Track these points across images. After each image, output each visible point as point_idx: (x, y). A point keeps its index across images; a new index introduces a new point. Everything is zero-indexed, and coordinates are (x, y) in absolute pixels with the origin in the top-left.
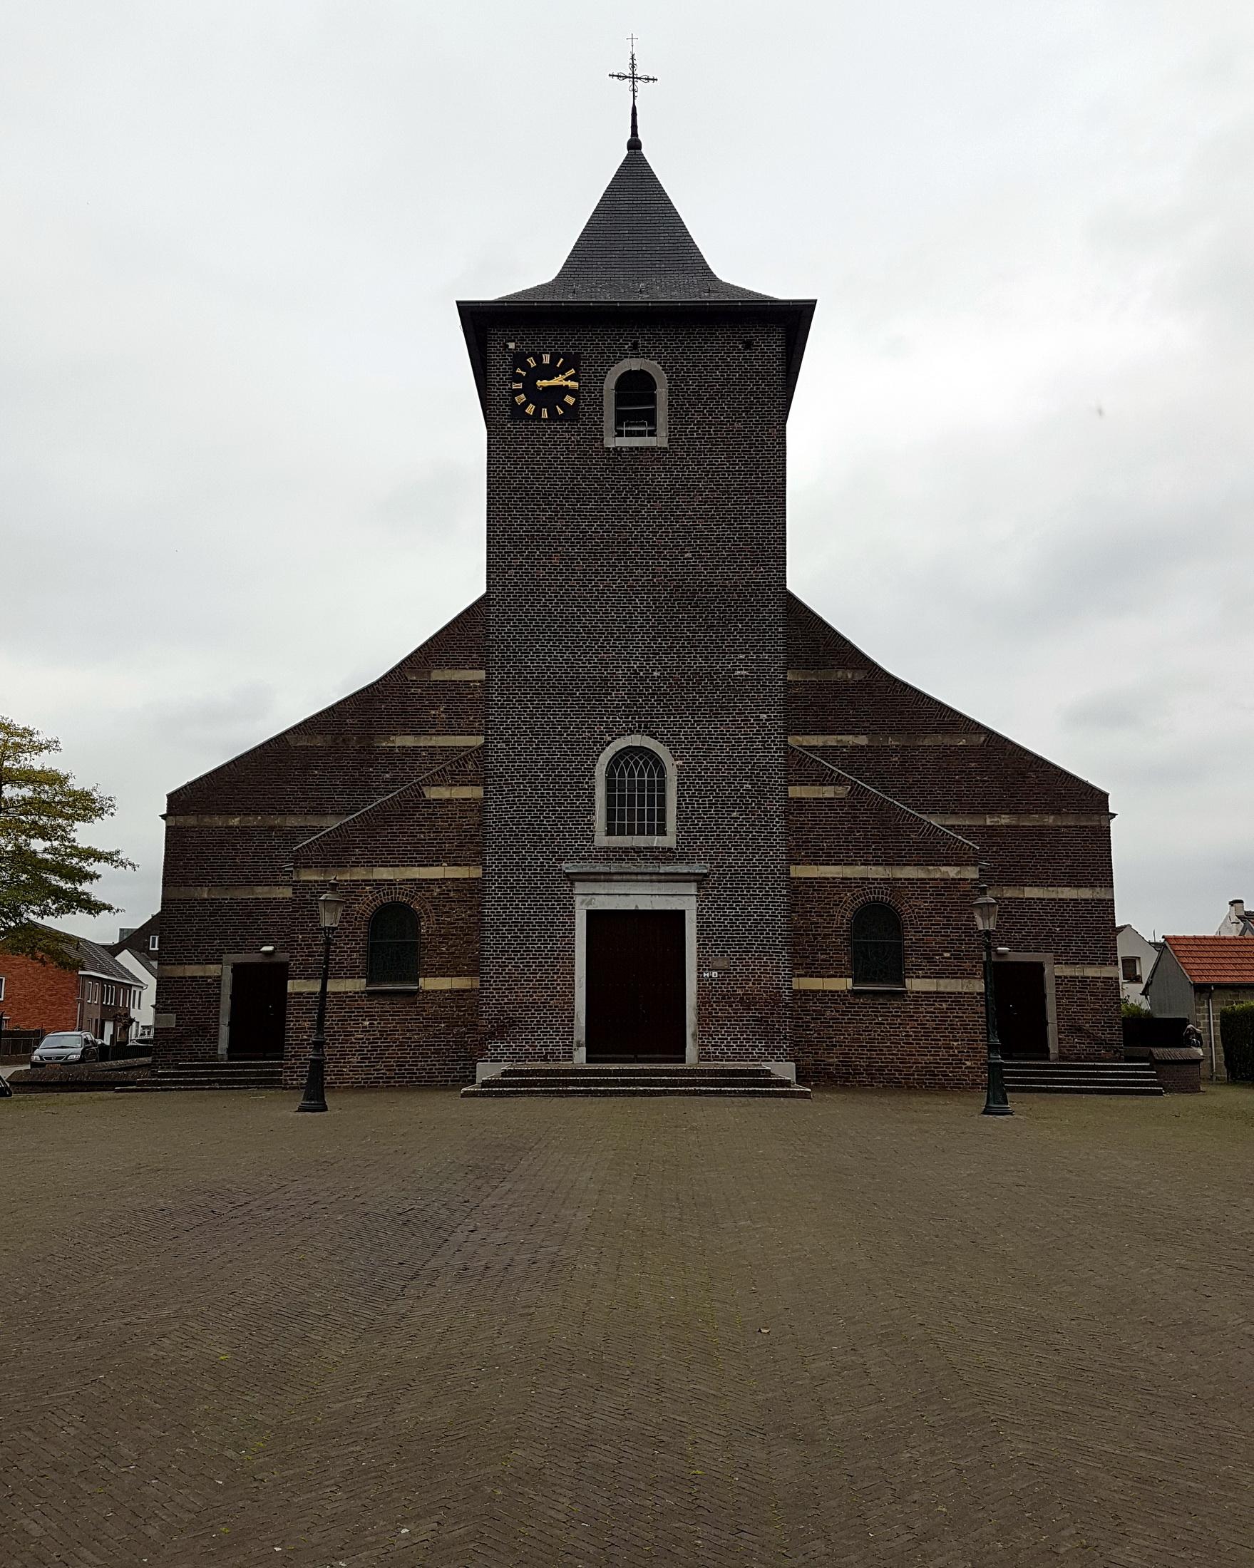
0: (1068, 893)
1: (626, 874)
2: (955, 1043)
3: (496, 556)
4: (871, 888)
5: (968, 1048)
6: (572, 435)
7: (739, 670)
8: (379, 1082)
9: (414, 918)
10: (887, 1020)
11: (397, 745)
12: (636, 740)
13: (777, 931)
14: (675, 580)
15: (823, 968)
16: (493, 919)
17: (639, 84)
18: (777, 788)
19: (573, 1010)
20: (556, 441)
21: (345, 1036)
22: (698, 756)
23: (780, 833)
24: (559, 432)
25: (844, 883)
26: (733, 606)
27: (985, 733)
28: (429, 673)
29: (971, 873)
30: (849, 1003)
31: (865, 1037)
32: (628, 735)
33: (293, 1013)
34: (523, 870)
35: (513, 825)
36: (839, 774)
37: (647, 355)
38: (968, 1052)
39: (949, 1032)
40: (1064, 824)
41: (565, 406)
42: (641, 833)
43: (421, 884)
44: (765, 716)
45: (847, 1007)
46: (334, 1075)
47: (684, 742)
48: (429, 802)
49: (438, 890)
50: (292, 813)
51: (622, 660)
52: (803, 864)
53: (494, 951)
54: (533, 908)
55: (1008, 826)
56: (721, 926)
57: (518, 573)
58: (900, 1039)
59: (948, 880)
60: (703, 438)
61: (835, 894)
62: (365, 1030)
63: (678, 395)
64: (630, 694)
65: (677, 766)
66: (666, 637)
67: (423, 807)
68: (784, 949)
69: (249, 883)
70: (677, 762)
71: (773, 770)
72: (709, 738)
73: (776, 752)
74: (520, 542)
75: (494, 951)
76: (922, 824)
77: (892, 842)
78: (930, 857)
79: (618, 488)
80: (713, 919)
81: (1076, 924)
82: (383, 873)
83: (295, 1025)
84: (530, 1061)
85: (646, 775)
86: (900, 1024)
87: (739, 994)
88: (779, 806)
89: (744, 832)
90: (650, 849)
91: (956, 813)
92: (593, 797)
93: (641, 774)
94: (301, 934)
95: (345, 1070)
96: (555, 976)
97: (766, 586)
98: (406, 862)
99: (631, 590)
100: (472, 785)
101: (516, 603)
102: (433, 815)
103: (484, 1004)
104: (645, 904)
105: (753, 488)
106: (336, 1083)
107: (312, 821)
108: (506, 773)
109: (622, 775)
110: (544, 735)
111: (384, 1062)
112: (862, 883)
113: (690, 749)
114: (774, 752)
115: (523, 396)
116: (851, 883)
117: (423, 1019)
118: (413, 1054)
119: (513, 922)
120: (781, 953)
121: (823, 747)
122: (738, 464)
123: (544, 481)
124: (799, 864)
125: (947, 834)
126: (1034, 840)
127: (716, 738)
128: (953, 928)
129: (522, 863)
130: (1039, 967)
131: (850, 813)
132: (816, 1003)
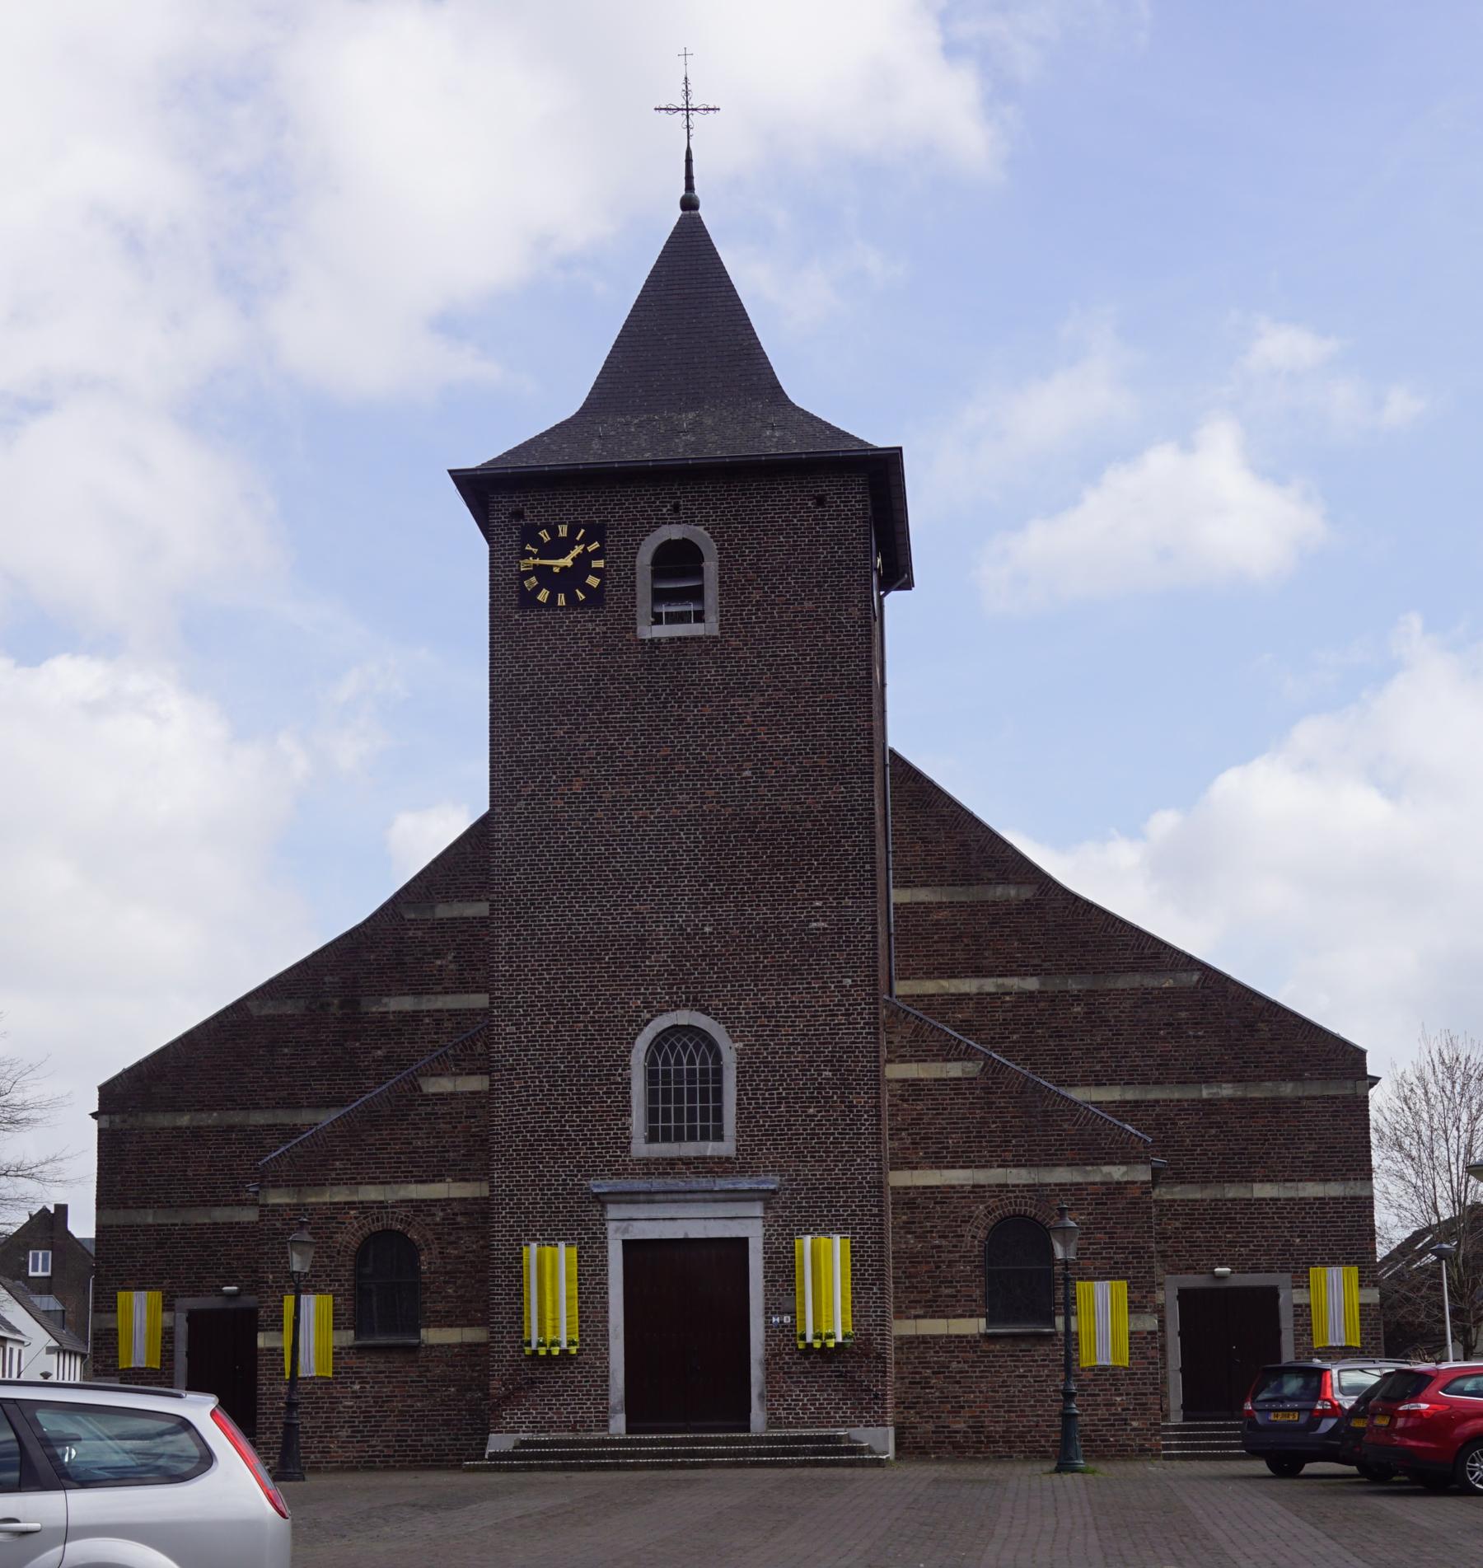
0: (1311, 1190)
1: (672, 1192)
2: (1118, 1399)
3: (502, 784)
4: (1010, 1197)
5: (1135, 1404)
6: (596, 625)
8: (375, 1462)
9: (412, 1251)
10: (1031, 1371)
12: (684, 1017)
13: (867, 1261)
14: (731, 806)
15: (947, 1306)
16: (504, 1254)
18: (866, 1076)
19: (607, 1367)
20: (576, 634)
21: (330, 1403)
23: (869, 1134)
24: (580, 622)
26: (806, 838)
28: (432, 908)
29: (1142, 1174)
30: (981, 1352)
31: (1001, 1395)
32: (673, 1010)
33: (265, 1375)
34: (540, 1190)
35: (527, 1132)
36: (968, 1045)
37: (690, 519)
38: (1134, 1409)
39: (1111, 1385)
40: (1306, 1094)
41: (587, 589)
42: (692, 1138)
43: (419, 1206)
44: (849, 981)
45: (979, 1357)
46: (319, 1452)
47: (745, 1018)
48: (427, 1098)
49: (441, 1214)
50: (257, 1107)
52: (922, 1168)
53: (506, 1294)
57: (530, 804)
58: (1047, 1396)
59: (1111, 1183)
60: (765, 622)
61: (963, 1207)
62: (356, 1396)
63: (731, 569)
64: (675, 957)
65: (737, 1050)
66: (720, 880)
67: (419, 1105)
68: (875, 1284)
69: (205, 1203)
70: (737, 1045)
74: (531, 765)
76: (1078, 1110)
77: (1038, 1135)
78: (1090, 1152)
79: (655, 691)
80: (784, 1248)
81: (1322, 1232)
82: (371, 1193)
83: (268, 1389)
84: (555, 1431)
85: (698, 1062)
86: (1047, 1376)
88: (869, 1098)
89: (823, 1134)
90: (703, 1159)
92: (628, 1093)
93: (691, 1061)
95: (332, 1446)
97: (848, 811)
98: (399, 1177)
99: (674, 821)
100: (481, 1074)
101: (527, 843)
103: (497, 1361)
104: (696, 1231)
105: (830, 684)
106: (322, 1462)
107: (284, 1117)
108: (517, 1065)
109: (666, 1062)
111: (381, 1436)
112: (1000, 1191)
113: (753, 1027)
114: (862, 1028)
115: (533, 579)
116: (985, 1192)
117: (428, 1381)
118: (417, 1426)
120: (872, 1289)
121: (978, 994)
122: (809, 654)
123: (561, 686)
125: (1111, 1122)
126: (1267, 1117)
127: (786, 1012)
128: (1117, 1248)
129: (540, 1181)
130: (1272, 1293)
131: (983, 1098)
132: (937, 1352)
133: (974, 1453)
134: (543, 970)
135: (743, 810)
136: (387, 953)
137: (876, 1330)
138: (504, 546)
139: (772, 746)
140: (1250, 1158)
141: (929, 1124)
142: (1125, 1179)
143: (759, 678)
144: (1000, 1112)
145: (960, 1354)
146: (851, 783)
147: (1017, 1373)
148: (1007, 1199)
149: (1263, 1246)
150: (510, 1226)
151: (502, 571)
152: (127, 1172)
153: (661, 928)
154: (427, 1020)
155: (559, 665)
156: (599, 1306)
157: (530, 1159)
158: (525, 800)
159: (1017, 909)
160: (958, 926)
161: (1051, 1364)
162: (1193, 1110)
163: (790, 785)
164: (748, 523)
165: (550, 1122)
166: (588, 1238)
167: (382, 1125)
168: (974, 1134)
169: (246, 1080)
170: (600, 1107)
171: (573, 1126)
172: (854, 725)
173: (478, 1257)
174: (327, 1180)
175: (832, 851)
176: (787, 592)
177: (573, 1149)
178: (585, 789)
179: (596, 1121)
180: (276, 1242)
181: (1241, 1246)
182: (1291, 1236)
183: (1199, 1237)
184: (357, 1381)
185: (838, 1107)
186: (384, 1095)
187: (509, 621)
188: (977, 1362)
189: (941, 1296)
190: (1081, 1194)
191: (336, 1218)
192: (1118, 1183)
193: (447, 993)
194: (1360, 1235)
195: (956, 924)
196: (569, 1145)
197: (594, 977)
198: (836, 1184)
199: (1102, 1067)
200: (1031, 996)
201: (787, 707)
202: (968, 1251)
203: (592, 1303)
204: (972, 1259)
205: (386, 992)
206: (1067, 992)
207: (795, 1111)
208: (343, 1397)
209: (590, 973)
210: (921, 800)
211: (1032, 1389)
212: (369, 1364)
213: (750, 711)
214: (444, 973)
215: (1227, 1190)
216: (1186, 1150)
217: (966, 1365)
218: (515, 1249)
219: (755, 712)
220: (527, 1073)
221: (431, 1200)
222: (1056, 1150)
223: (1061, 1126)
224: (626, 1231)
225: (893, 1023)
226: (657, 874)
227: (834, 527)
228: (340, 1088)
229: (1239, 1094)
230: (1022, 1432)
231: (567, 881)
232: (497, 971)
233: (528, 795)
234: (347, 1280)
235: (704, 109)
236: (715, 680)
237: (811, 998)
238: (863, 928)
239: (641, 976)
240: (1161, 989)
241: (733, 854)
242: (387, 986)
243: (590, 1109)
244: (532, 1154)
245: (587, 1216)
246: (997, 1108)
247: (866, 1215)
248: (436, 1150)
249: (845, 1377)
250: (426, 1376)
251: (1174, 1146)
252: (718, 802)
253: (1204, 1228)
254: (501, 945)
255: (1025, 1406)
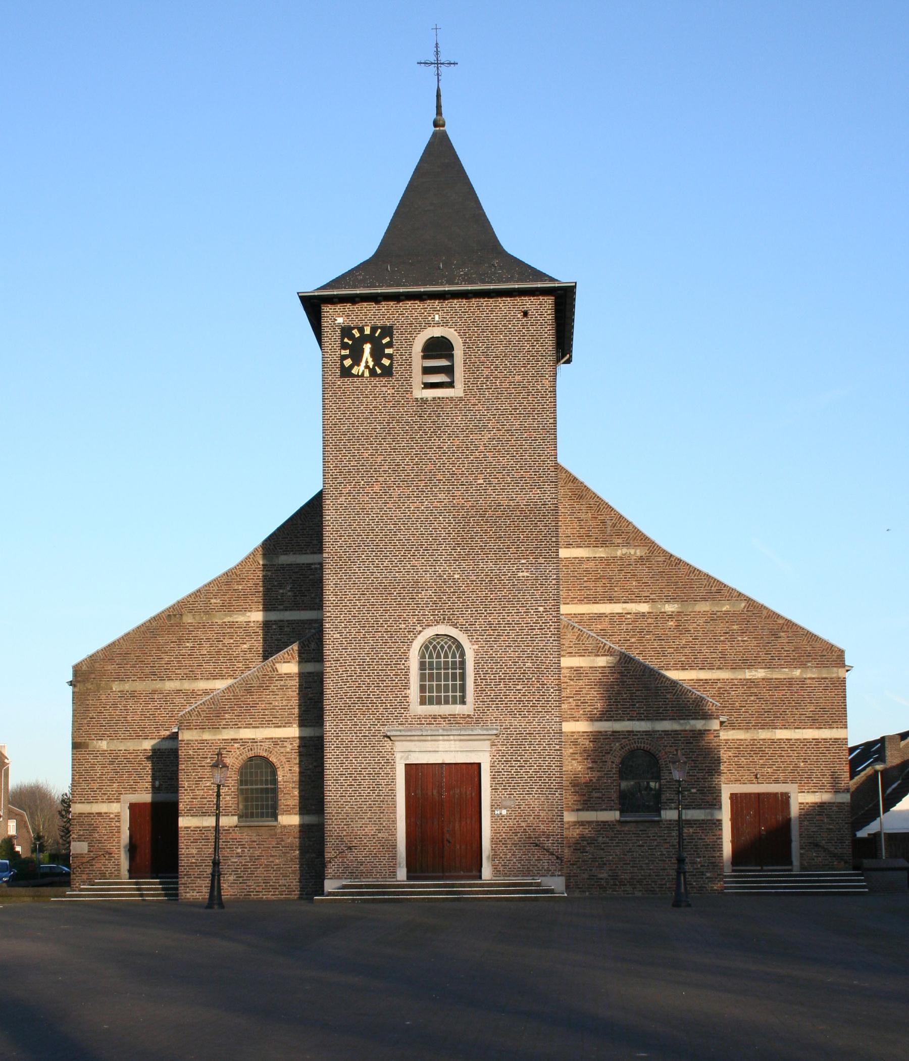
2: (698, 860)
5: (709, 863)
7: (522, 572)
8: (250, 895)
10: (646, 843)
11: (252, 620)
12: (443, 629)
15: (596, 804)
16: (333, 772)
17: (443, 68)
22: (490, 641)
24: (378, 387)
25: (613, 735)
27: (745, 600)
32: (435, 625)
34: (355, 733)
38: (708, 866)
39: (694, 851)
42: (447, 702)
45: (615, 834)
49: (290, 746)
51: (429, 566)
54: (363, 763)
55: (763, 679)
56: (509, 775)
57: (347, 499)
65: (474, 650)
67: (276, 680)
68: (557, 791)
71: (548, 651)
72: (499, 627)
73: (551, 637)
75: (334, 796)
76: (676, 686)
80: (502, 769)
82: (246, 734)
85: (450, 657)
86: (657, 846)
87: (523, 827)
88: (554, 679)
89: (526, 701)
91: (721, 669)
93: (446, 656)
94: (187, 781)
96: (382, 815)
102: (284, 686)
107: (187, 685)
109: (431, 657)
110: (369, 627)
111: (254, 880)
116: (619, 735)
117: (282, 847)
118: (276, 874)
119: (348, 774)
120: (555, 794)
124: (578, 721)
126: (784, 690)
128: (699, 770)
130: (785, 798)
133: (612, 891)
134: (356, 600)
135: (478, 503)
136: (249, 585)
137: (557, 819)
138: (331, 339)
139: (496, 465)
140: (774, 714)
141: (586, 694)
142: (704, 728)
143: (488, 423)
144: (629, 687)
145: (604, 833)
146: (543, 488)
147: (638, 844)
148: (633, 739)
149: (781, 767)
150: (337, 755)
151: (330, 355)
152: (90, 718)
153: (428, 575)
154: (274, 627)
155: (365, 413)
156: (390, 803)
157: (349, 714)
158: (344, 496)
159: (635, 562)
160: (599, 572)
161: (658, 839)
162: (741, 685)
163: (507, 489)
164: (481, 327)
165: (361, 692)
166: (384, 763)
167: (254, 692)
168: (614, 700)
169: (164, 662)
170: (391, 683)
171: (374, 695)
172: (546, 452)
173: (313, 772)
174: (220, 725)
175: (532, 529)
176: (505, 370)
177: (375, 709)
178: (381, 490)
179: (389, 692)
180: (189, 762)
181: (768, 768)
182: (798, 762)
183: (743, 762)
184: (239, 847)
185: (535, 684)
186: (255, 674)
187: (334, 385)
188: (615, 837)
189: (592, 798)
190: (678, 737)
191: (226, 748)
192: (700, 730)
193: (286, 610)
194: (839, 761)
195: (598, 571)
196: (372, 706)
197: (387, 605)
198: (534, 731)
199: (686, 658)
200: (643, 615)
201: (505, 441)
202: (609, 771)
203: (387, 801)
204: (612, 775)
205: (249, 609)
206: (665, 613)
207: (509, 687)
208: (231, 856)
209: (385, 602)
210: (576, 494)
211: (647, 854)
212: (247, 837)
213: (482, 443)
214: (284, 598)
215: (760, 733)
216: (736, 709)
217: (608, 839)
218: (339, 769)
219: (485, 444)
220: (346, 663)
221: (284, 738)
222: (663, 710)
223: (666, 696)
224: (407, 758)
225: (565, 633)
226: (425, 542)
227: (534, 330)
228: (221, 668)
229: (769, 676)
230: (641, 879)
231: (370, 546)
232: (328, 601)
233: (346, 493)
234: (233, 786)
235: (448, 64)
236: (461, 424)
237: (519, 618)
238: (551, 576)
239: (416, 604)
240: (721, 611)
241: (472, 531)
242: (249, 605)
243: (385, 685)
244: (350, 712)
245: (384, 749)
246: (627, 685)
247: (552, 750)
248: (287, 707)
249: (539, 846)
250: (281, 844)
251: (728, 707)
252: (463, 499)
253: (747, 756)
254: (330, 585)
255: (642, 864)
